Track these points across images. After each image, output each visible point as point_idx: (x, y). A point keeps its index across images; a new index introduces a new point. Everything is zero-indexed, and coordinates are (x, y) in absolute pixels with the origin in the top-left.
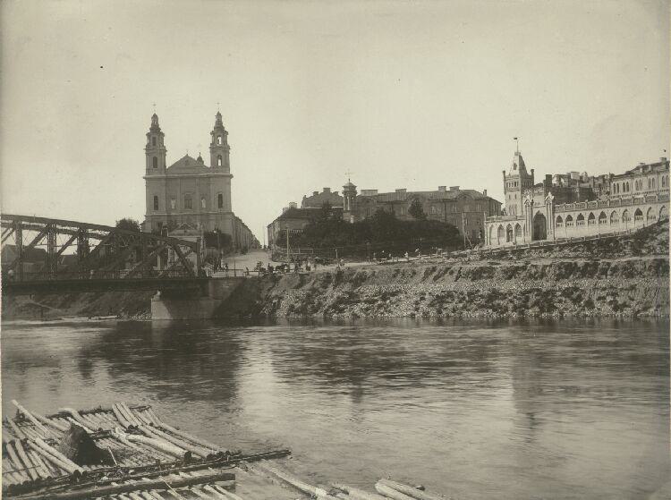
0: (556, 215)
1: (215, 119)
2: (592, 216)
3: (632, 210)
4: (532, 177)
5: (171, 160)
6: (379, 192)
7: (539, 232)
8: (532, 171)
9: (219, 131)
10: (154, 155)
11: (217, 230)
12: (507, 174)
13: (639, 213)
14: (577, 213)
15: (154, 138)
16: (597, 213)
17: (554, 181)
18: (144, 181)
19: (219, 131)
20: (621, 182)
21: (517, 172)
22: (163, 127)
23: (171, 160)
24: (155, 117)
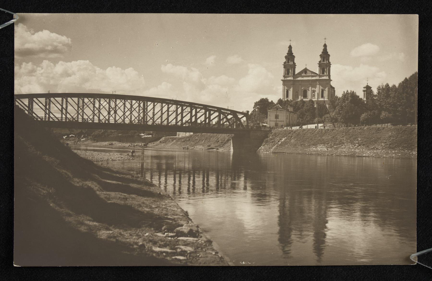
9: (325, 55)
19: (325, 55)
22: (293, 51)
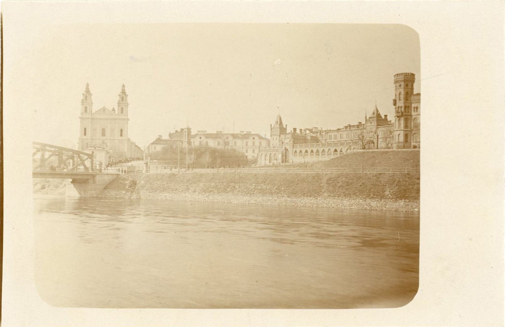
0: (294, 150)
1: (85, 87)
2: (312, 151)
3: (332, 149)
4: (286, 129)
5: (95, 108)
6: (208, 133)
7: (285, 158)
8: (386, 116)
9: (123, 95)
10: (86, 105)
11: (386, 116)
12: (272, 127)
13: (336, 151)
14: (311, 149)
15: (86, 96)
16: (321, 150)
17: (298, 131)
18: (79, 120)
19: (123, 95)
20: (333, 134)
21: (278, 126)
23: (95, 108)
24: (124, 86)
